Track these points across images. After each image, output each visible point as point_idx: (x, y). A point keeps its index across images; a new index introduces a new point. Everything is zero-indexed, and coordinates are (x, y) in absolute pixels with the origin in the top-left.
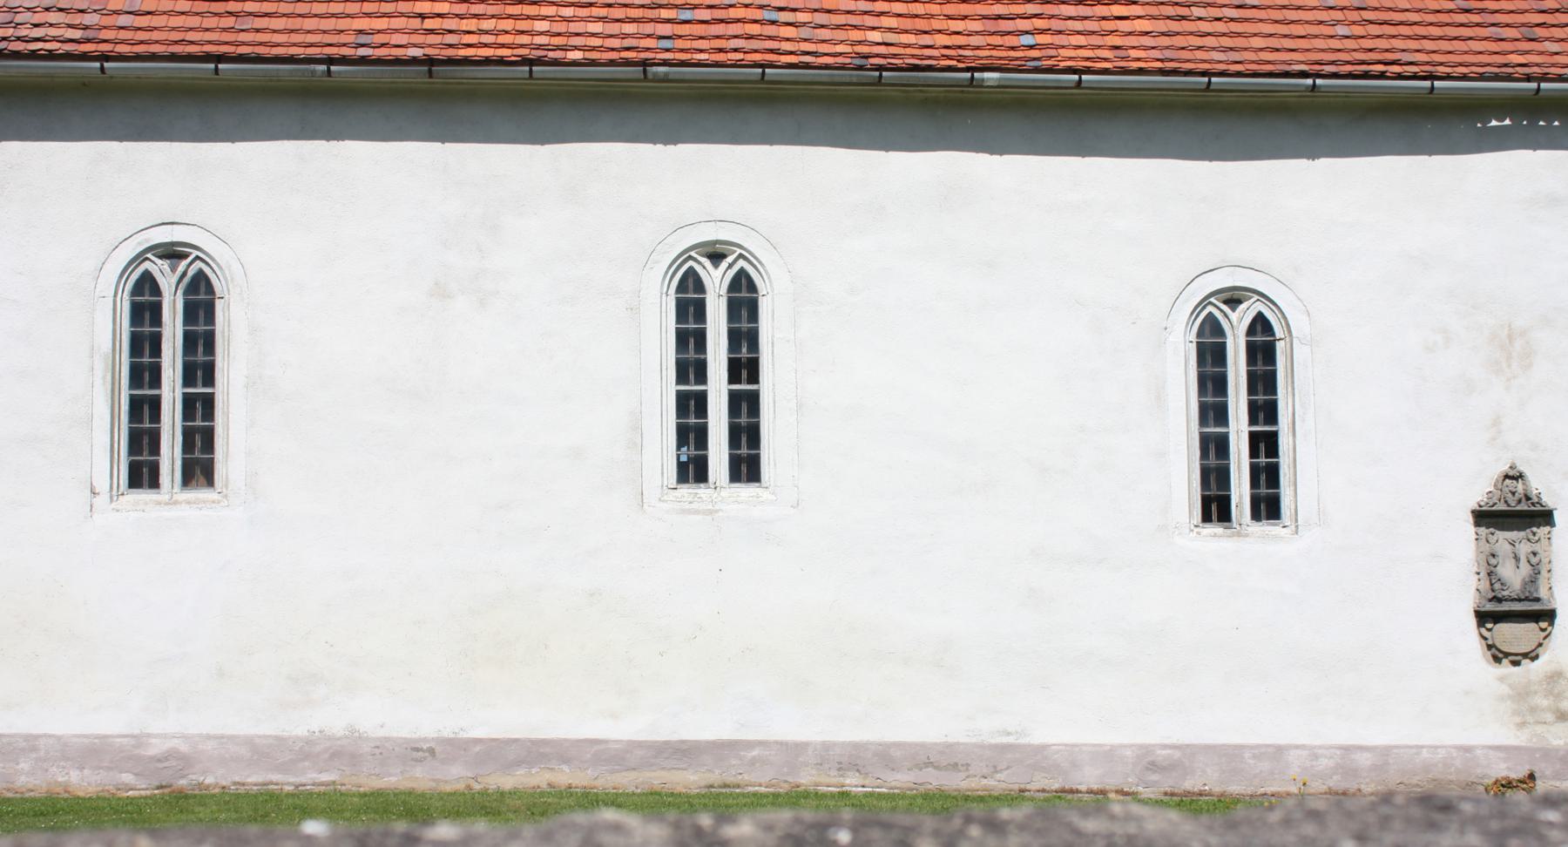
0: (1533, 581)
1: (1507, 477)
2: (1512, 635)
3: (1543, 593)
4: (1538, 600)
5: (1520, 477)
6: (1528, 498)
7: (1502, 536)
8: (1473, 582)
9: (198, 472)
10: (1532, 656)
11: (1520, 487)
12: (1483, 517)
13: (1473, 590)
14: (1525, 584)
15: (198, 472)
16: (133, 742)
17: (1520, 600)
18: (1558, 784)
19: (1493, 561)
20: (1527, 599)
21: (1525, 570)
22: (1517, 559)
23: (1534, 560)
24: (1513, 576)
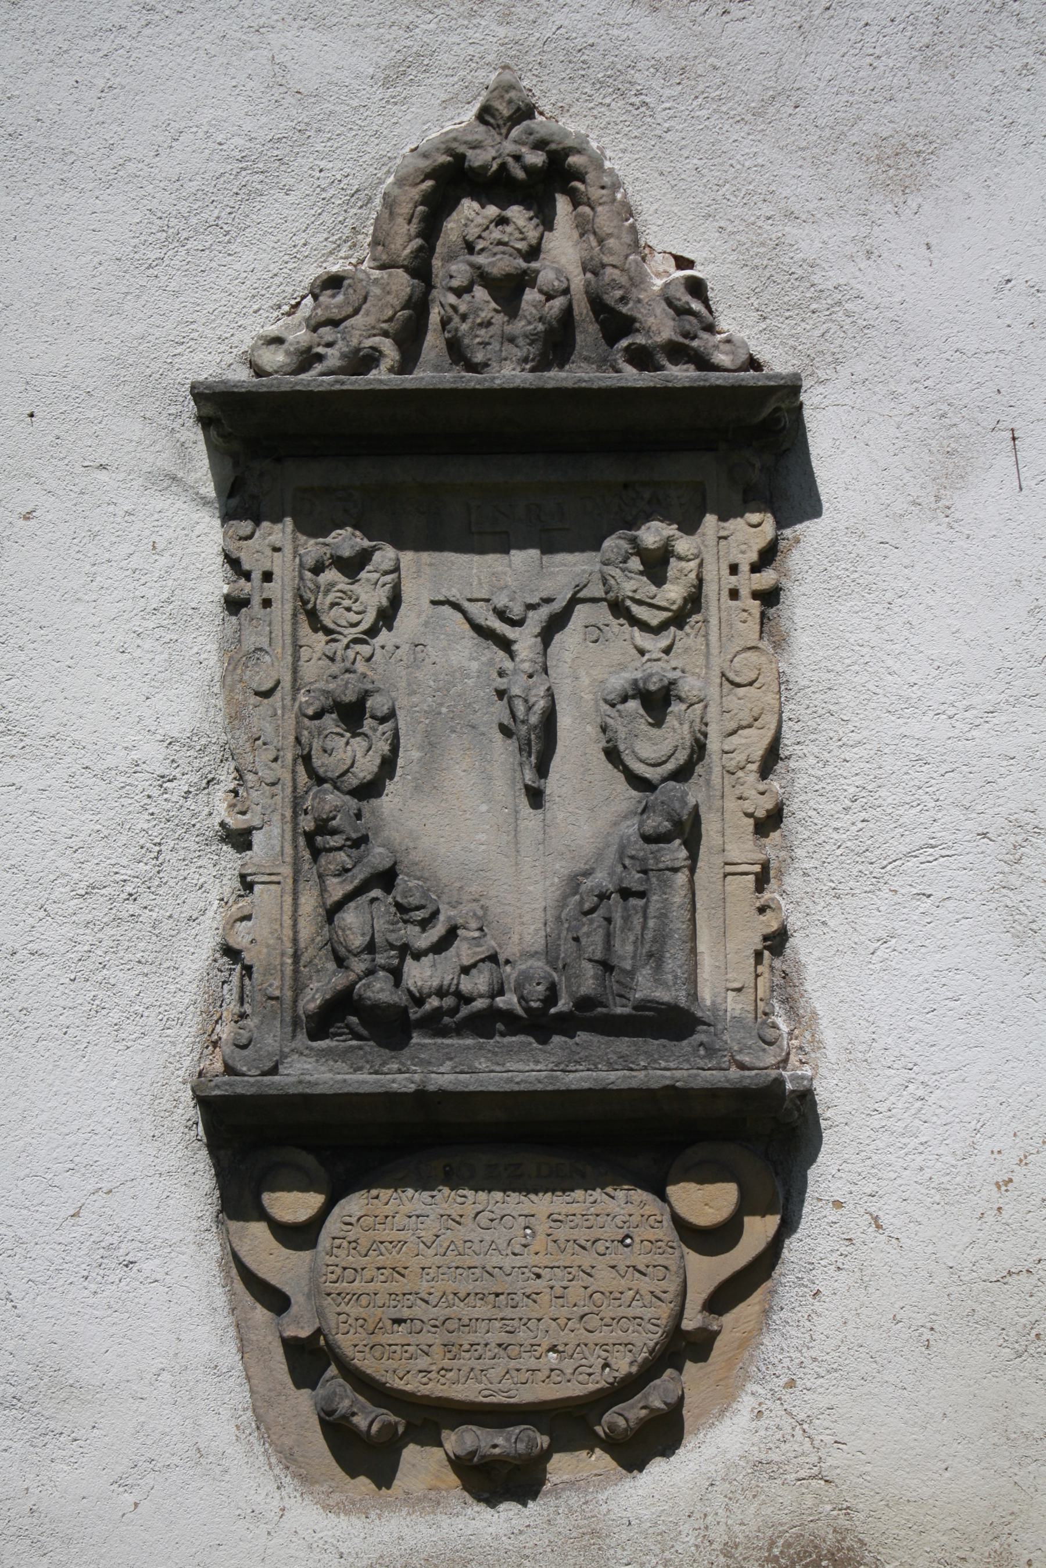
20: (588, 1017)
24: (497, 855)
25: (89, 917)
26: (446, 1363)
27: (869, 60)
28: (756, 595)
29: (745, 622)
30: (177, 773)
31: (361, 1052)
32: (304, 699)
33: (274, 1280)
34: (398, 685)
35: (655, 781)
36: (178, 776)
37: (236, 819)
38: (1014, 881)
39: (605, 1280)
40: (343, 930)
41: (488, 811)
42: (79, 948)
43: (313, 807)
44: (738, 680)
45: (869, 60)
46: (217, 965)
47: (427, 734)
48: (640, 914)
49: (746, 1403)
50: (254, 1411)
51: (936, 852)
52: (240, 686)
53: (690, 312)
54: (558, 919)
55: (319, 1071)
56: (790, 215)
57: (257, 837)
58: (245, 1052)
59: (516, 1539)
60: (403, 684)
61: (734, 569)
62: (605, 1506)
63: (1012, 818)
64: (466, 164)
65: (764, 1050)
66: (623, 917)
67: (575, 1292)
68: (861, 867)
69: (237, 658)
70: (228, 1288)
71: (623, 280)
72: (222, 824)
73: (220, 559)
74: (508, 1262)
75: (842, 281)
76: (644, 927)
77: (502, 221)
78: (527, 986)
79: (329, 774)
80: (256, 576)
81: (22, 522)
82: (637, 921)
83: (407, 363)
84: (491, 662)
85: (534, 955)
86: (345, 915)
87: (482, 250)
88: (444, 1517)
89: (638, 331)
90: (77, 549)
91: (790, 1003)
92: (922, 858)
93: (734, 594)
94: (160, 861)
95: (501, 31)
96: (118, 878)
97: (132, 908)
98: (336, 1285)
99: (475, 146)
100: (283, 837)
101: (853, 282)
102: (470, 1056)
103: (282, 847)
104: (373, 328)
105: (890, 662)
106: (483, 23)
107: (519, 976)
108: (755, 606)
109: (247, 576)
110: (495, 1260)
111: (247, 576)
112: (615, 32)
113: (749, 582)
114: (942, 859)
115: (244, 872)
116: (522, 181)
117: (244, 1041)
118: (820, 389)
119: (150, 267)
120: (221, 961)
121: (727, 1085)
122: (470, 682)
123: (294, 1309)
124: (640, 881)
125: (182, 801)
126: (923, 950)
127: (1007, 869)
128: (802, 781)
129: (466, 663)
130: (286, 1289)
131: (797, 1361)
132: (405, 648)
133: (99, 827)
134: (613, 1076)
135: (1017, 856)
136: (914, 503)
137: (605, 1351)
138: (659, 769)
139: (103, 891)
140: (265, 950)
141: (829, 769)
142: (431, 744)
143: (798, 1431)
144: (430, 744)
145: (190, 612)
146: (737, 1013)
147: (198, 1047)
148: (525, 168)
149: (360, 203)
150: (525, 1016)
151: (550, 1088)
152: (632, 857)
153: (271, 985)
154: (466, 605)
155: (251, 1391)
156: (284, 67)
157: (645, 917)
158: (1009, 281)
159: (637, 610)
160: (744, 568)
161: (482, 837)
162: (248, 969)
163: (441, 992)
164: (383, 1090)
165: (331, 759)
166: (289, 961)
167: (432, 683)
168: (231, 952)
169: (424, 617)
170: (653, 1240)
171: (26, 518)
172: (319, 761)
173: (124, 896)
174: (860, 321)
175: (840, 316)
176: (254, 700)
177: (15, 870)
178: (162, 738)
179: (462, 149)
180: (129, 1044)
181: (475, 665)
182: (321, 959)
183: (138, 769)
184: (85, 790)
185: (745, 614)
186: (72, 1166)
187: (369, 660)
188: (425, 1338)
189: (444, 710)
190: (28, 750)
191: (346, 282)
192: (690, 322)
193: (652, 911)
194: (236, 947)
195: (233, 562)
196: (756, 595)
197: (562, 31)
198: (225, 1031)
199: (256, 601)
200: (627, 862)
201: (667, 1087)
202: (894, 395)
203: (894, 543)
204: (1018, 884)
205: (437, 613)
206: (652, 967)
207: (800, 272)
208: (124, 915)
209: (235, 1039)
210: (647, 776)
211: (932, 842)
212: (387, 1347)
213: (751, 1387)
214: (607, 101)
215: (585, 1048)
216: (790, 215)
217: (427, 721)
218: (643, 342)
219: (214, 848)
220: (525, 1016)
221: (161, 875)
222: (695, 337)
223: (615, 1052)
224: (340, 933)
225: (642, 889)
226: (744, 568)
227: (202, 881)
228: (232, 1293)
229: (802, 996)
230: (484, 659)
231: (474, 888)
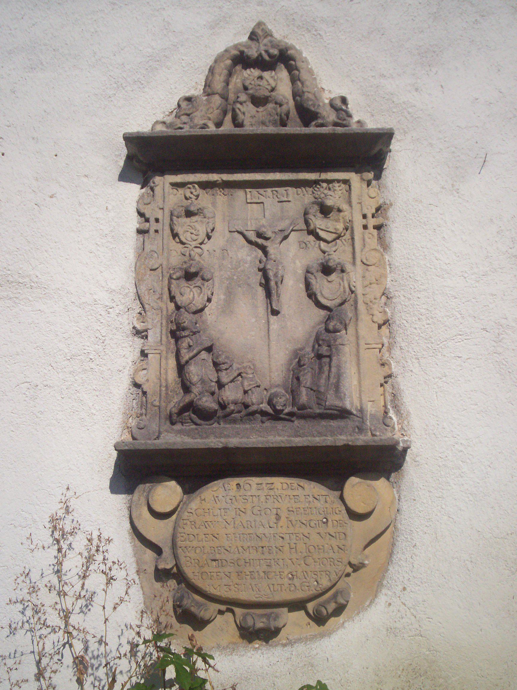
0: (321, 351)
1: (241, 60)
2: (249, 520)
3: (357, 388)
4: (343, 414)
5: (284, 59)
6: (307, 115)
7: (219, 208)
8: (123, 354)
9: (191, 410)
10: (324, 609)
11: (280, 82)
12: (150, 157)
13: (126, 382)
14: (297, 364)
15: (191, 410)
16: (338, 413)
17: (275, 416)
18: (271, 438)
19: (190, 294)
20: (302, 414)
21: (298, 321)
22: (268, 286)
23: (328, 289)
24: (258, 340)
25: (72, 369)
26: (238, 581)
27: (413, 17)
28: (375, 227)
29: (369, 238)
30: (114, 305)
31: (197, 431)
32: (172, 272)
33: (154, 540)
34: (215, 267)
35: (366, 182)
36: (115, 306)
37: (140, 325)
38: (499, 350)
39: (315, 539)
40: (189, 374)
41: (256, 321)
42: (66, 383)
43: (175, 319)
44: (368, 263)
45: (413, 17)
46: (130, 391)
47: (228, 288)
48: (327, 366)
49: (382, 599)
50: (144, 604)
51: (463, 337)
52: (143, 266)
53: (342, 109)
54: (288, 370)
55: (176, 438)
56: (383, 76)
57: (150, 333)
58: (143, 431)
59: (272, 668)
60: (216, 267)
61: (365, 216)
62: (315, 651)
63: (497, 322)
64: (245, 55)
65: (386, 430)
66: (319, 368)
67: (301, 547)
68: (428, 345)
69: (141, 253)
70: (133, 544)
71: (313, 98)
72: (134, 328)
73: (136, 214)
74: (267, 531)
75: (406, 100)
76: (330, 371)
77: (261, 78)
78: (275, 399)
79: (183, 305)
80: (152, 220)
81: (49, 199)
82: (326, 368)
83: (219, 125)
84: (256, 257)
85: (278, 386)
86: (189, 367)
87: (252, 88)
88: (237, 657)
89: (320, 117)
90: (73, 209)
91: (397, 408)
92: (456, 340)
93: (365, 227)
94: (105, 344)
95: (259, 8)
96: (85, 351)
97: (92, 365)
98: (184, 543)
99: (249, 47)
100: (161, 333)
101: (410, 100)
102: (248, 433)
103: (161, 338)
104: (204, 116)
105: (436, 255)
106: (251, 5)
107: (271, 395)
108: (375, 232)
109: (147, 220)
110: (261, 530)
111: (147, 220)
112: (306, 8)
113: (372, 222)
114: (465, 341)
115: (143, 349)
116: (269, 62)
117: (142, 426)
118: (398, 144)
119: (110, 97)
120: (132, 390)
121: (374, 444)
122: (247, 265)
123: (164, 554)
124: (327, 350)
125: (116, 317)
126: (459, 382)
127: (495, 345)
128: (399, 307)
129: (244, 257)
130: (160, 545)
131: (407, 578)
132: (218, 251)
133: (77, 329)
134: (317, 439)
135: (500, 339)
136: (443, 188)
137: (315, 574)
138: (334, 302)
139: (79, 358)
140: (152, 384)
141: (411, 302)
142: (230, 293)
143: (408, 614)
144: (229, 292)
145: (122, 235)
146: (373, 412)
147: (120, 430)
148: (270, 55)
149: (199, 73)
150: (273, 413)
151: (288, 445)
152: (323, 340)
153: (155, 400)
154: (246, 233)
155: (143, 594)
156: (169, 23)
157: (330, 367)
158: (477, 99)
159: (322, 234)
160: (369, 216)
161: (253, 333)
162: (144, 393)
163: (235, 403)
164: (207, 447)
165: (184, 298)
166: (164, 389)
167: (230, 266)
168: (137, 385)
169: (226, 239)
170: (337, 520)
171: (51, 197)
172: (178, 299)
173: (88, 360)
174: (414, 116)
175: (406, 114)
176: (149, 272)
177: (39, 348)
178: (107, 289)
179: (242, 49)
180: (88, 428)
181: (249, 258)
182: (178, 388)
183: (96, 303)
184: (72, 312)
185: (370, 235)
186: (60, 485)
187: (200, 256)
188: (227, 569)
189: (235, 278)
190: (47, 295)
191: (193, 100)
192: (342, 114)
193: (334, 363)
194: (139, 383)
195: (141, 214)
196: (375, 227)
197: (284, 8)
198: (132, 422)
199: (152, 231)
200: (321, 342)
201: (345, 445)
202: (431, 145)
203: (435, 204)
204: (501, 351)
205: (230, 215)
206: (333, 391)
207: (387, 97)
208: (88, 368)
209: (137, 425)
210: (329, 305)
211: (460, 333)
212: (209, 573)
213: (384, 591)
214: (304, 33)
215: (302, 429)
216: (383, 76)
217: (228, 282)
218: (322, 122)
219: (130, 339)
220: (273, 413)
221: (105, 350)
222: (345, 120)
223: (316, 431)
224: (187, 375)
225: (328, 354)
226: (369, 216)
227: (124, 353)
228: (135, 546)
229: (402, 404)
230: (253, 256)
231: (250, 356)
